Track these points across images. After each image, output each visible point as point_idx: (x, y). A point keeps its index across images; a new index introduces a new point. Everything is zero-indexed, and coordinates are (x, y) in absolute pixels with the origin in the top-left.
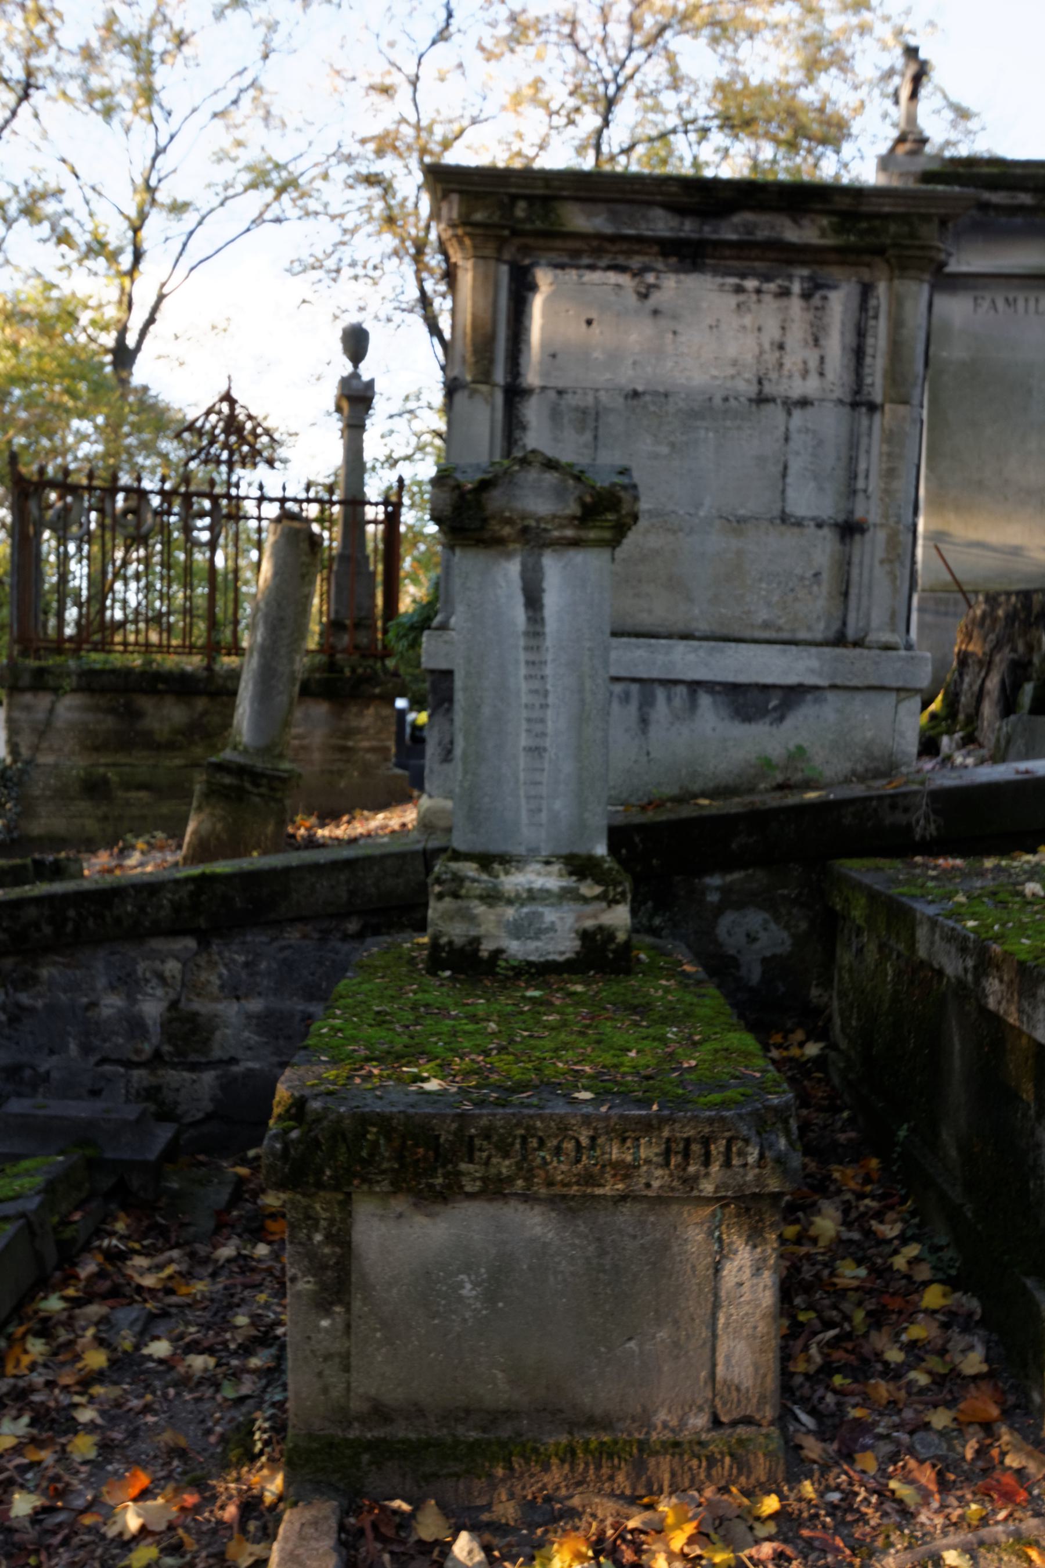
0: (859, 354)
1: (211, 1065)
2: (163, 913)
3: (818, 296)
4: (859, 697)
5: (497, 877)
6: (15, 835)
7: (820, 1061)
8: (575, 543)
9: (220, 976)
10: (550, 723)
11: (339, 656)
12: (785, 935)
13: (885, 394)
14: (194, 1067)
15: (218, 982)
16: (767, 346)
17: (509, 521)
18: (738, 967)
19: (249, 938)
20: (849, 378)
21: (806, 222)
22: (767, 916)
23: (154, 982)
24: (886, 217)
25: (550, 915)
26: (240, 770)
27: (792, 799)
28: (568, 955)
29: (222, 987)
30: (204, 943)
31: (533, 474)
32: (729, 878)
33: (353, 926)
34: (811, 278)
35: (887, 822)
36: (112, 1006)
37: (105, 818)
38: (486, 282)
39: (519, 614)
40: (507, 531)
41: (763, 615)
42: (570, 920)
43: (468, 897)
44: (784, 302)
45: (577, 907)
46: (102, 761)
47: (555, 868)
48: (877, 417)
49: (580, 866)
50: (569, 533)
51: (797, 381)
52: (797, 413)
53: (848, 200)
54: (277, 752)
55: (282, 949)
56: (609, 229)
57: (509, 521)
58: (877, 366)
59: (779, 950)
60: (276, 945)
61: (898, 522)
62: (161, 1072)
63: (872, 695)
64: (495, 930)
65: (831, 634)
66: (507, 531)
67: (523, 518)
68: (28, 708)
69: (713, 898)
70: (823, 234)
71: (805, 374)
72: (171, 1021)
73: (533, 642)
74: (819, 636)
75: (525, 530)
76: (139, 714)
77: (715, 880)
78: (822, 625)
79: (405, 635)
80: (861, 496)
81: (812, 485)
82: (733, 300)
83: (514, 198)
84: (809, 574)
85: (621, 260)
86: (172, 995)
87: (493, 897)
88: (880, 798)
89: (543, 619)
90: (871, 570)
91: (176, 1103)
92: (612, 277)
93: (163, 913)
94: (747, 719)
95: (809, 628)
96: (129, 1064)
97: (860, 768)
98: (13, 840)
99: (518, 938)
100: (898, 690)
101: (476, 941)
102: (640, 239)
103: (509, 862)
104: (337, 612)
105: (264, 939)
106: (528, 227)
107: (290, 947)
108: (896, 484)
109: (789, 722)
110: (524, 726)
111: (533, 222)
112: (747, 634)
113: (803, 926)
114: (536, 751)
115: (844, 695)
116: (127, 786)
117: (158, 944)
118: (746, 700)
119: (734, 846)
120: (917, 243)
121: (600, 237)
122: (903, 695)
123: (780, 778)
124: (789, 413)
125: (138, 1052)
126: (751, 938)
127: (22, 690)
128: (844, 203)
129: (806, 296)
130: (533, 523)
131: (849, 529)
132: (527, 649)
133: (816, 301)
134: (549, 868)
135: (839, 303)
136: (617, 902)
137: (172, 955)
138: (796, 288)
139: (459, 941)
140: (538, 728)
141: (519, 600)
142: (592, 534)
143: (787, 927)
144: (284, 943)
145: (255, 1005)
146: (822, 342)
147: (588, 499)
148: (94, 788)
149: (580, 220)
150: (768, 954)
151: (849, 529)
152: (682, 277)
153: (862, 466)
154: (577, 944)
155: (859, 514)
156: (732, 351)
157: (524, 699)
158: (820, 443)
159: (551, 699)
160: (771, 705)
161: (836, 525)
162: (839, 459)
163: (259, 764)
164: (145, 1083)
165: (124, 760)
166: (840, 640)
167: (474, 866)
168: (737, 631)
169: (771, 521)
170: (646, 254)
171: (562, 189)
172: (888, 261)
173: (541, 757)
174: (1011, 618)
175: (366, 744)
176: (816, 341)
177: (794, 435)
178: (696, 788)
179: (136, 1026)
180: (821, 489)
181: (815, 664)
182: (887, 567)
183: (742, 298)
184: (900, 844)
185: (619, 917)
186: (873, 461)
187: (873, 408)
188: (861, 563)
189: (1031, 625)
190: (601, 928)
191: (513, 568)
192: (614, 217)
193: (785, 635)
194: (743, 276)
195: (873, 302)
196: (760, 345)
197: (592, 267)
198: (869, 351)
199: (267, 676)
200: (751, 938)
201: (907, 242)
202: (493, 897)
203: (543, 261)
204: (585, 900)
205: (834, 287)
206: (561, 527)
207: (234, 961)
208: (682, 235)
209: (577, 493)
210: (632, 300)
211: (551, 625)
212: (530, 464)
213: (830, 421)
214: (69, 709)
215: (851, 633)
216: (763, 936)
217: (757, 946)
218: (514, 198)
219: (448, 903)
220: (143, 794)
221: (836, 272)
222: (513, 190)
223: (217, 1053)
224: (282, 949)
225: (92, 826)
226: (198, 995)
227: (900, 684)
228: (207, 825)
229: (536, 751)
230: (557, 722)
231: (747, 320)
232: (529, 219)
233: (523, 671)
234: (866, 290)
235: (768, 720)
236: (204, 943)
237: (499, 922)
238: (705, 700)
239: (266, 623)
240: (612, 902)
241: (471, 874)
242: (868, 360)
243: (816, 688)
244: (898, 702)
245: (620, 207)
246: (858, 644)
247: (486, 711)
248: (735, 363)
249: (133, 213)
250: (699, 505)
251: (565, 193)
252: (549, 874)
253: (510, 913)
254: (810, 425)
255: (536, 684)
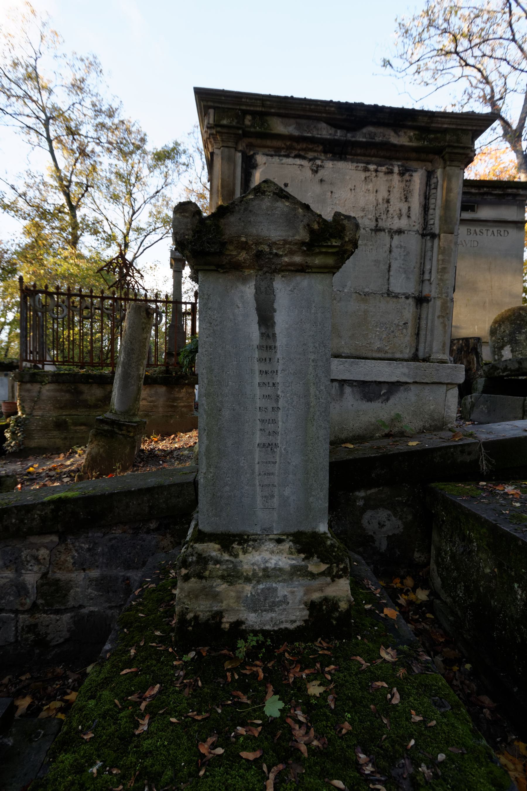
0: (426, 208)
1: (66, 611)
2: (35, 523)
3: (407, 174)
4: (427, 387)
5: (236, 556)
6: (22, 448)
7: (429, 605)
8: (302, 269)
9: (73, 557)
10: (280, 423)
11: (170, 367)
12: (400, 523)
13: (440, 229)
14: (57, 612)
15: (72, 561)
16: (380, 201)
17: (244, 246)
18: (374, 541)
19: (90, 535)
20: (421, 221)
21: (401, 133)
22: (389, 512)
23: (33, 562)
24: (445, 131)
25: (282, 590)
26: (113, 423)
27: (401, 448)
28: (298, 624)
29: (74, 564)
30: (63, 539)
31: (266, 202)
32: (369, 492)
33: (153, 525)
34: (402, 166)
35: (459, 460)
36: (6, 577)
37: (65, 438)
38: (229, 160)
39: (254, 331)
40: (243, 256)
41: (378, 344)
42: (300, 593)
43: (211, 577)
44: (390, 177)
45: (306, 581)
46: (64, 413)
47: (287, 545)
48: (436, 241)
49: (306, 544)
50: (298, 259)
51: (396, 220)
52: (396, 237)
53: (426, 119)
54: (131, 413)
55: (110, 540)
56: (296, 133)
57: (244, 246)
58: (436, 214)
59: (396, 532)
60: (107, 537)
61: (447, 296)
62: (37, 615)
63: (435, 387)
64: (235, 604)
65: (411, 355)
66: (243, 256)
67: (257, 244)
68: (28, 391)
69: (361, 503)
70: (411, 141)
71: (400, 216)
72: (42, 585)
73: (265, 355)
74: (406, 356)
75: (259, 255)
76: (81, 393)
77: (362, 494)
78: (408, 351)
79: (187, 356)
80: (427, 283)
81: (404, 276)
82: (363, 175)
83: (245, 113)
84: (401, 323)
85: (302, 153)
86: (44, 570)
87: (232, 576)
88: (455, 447)
89: (274, 335)
90: (433, 321)
91: (47, 634)
92: (298, 161)
93: (35, 523)
94: (370, 400)
95: (401, 352)
96: (17, 612)
97: (427, 425)
98: (20, 450)
99: (255, 611)
100: (447, 384)
101: (219, 614)
102: (313, 140)
103: (247, 541)
104: (169, 349)
105: (99, 534)
106: (252, 130)
107: (115, 538)
108: (446, 276)
109: (391, 401)
110: (259, 426)
111: (255, 128)
112: (369, 355)
113: (410, 517)
114: (269, 447)
115: (420, 387)
116: (75, 424)
117: (34, 539)
118: (370, 390)
119: (373, 475)
120: (461, 145)
121: (291, 138)
122: (450, 386)
123: (387, 431)
124: (392, 238)
125: (22, 605)
126: (381, 525)
127: (26, 383)
128: (422, 122)
129: (401, 174)
130: (267, 249)
131: (421, 300)
132: (260, 360)
133: (407, 177)
134: (281, 547)
135: (418, 179)
136: (340, 577)
137: (43, 547)
138: (396, 170)
139: (203, 617)
140: (271, 427)
141: (254, 318)
142: (318, 261)
143: (400, 519)
144: (112, 536)
145: (95, 573)
146: (409, 200)
147: (316, 227)
148: (60, 425)
149: (280, 127)
150: (391, 534)
151: (421, 300)
152: (335, 162)
153: (428, 267)
154: (306, 612)
155: (426, 292)
156: (362, 203)
157: (259, 403)
158: (408, 254)
159: (281, 403)
160: (382, 392)
161: (415, 297)
162: (416, 263)
163: (122, 419)
164: (27, 623)
165: (74, 413)
166: (415, 358)
167: (217, 546)
168: (364, 354)
169: (382, 295)
170: (315, 151)
171: (271, 107)
172: (443, 157)
173: (273, 452)
174: (460, 350)
175: (182, 404)
176: (406, 198)
177: (394, 249)
178: (343, 436)
179: (21, 589)
180: (408, 278)
181: (406, 370)
182: (441, 320)
183: (368, 174)
184: (469, 473)
185: (341, 589)
186: (433, 265)
187: (433, 236)
188: (427, 318)
189: (469, 353)
190: (326, 599)
191: (249, 290)
192: (299, 127)
193: (389, 356)
194: (368, 163)
195: (434, 180)
196: (377, 200)
197: (287, 156)
198: (432, 206)
199: (126, 376)
200: (381, 525)
201: (456, 144)
202: (232, 576)
203: (260, 153)
204: (313, 576)
205: (416, 171)
206: (292, 253)
207: (82, 548)
208: (336, 137)
209: (306, 221)
210: (309, 173)
211: (281, 341)
212: (264, 193)
213: (413, 242)
214: (48, 391)
215: (421, 355)
216: (387, 523)
217: (385, 529)
218: (245, 113)
219: (193, 583)
220: (82, 428)
221: (413, 164)
222: (244, 108)
223: (71, 603)
224: (110, 540)
225: (59, 442)
226: (60, 569)
227: (449, 381)
228: (95, 450)
229: (269, 447)
230: (286, 422)
231: (370, 186)
232: (252, 126)
233: (257, 379)
234: (430, 174)
235: (380, 400)
236: (63, 539)
237: (238, 597)
238: (348, 390)
239: (125, 351)
240: (335, 577)
241: (214, 554)
242: (431, 211)
243: (407, 383)
244: (447, 390)
245: (304, 121)
246: (424, 360)
247: (226, 413)
248: (363, 210)
249: (125, 232)
250: (344, 286)
251: (273, 111)
252: (280, 552)
253: (248, 589)
254: (402, 244)
255: (269, 391)
